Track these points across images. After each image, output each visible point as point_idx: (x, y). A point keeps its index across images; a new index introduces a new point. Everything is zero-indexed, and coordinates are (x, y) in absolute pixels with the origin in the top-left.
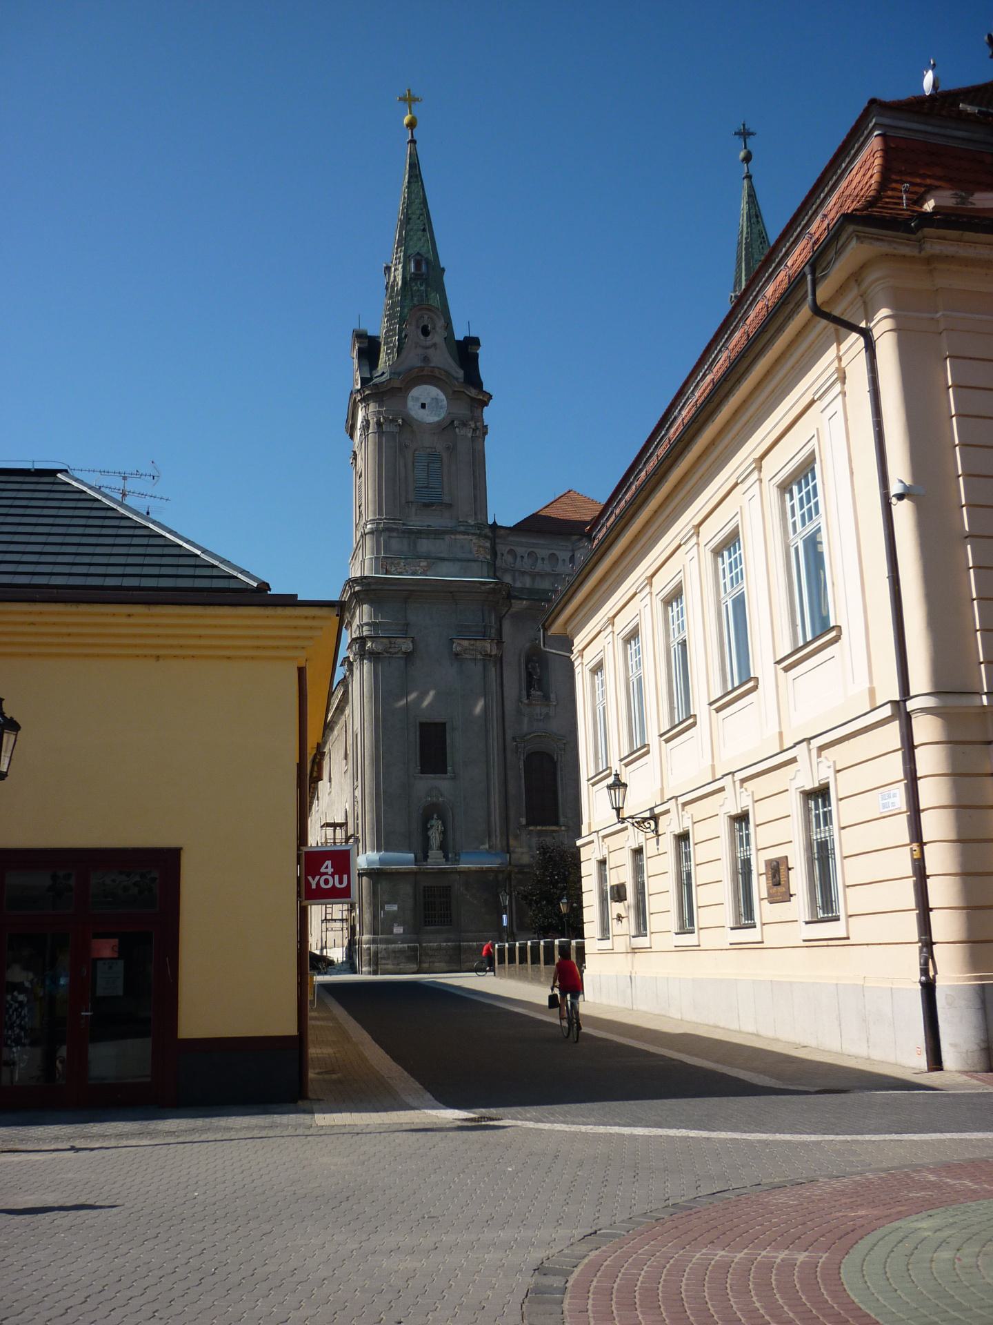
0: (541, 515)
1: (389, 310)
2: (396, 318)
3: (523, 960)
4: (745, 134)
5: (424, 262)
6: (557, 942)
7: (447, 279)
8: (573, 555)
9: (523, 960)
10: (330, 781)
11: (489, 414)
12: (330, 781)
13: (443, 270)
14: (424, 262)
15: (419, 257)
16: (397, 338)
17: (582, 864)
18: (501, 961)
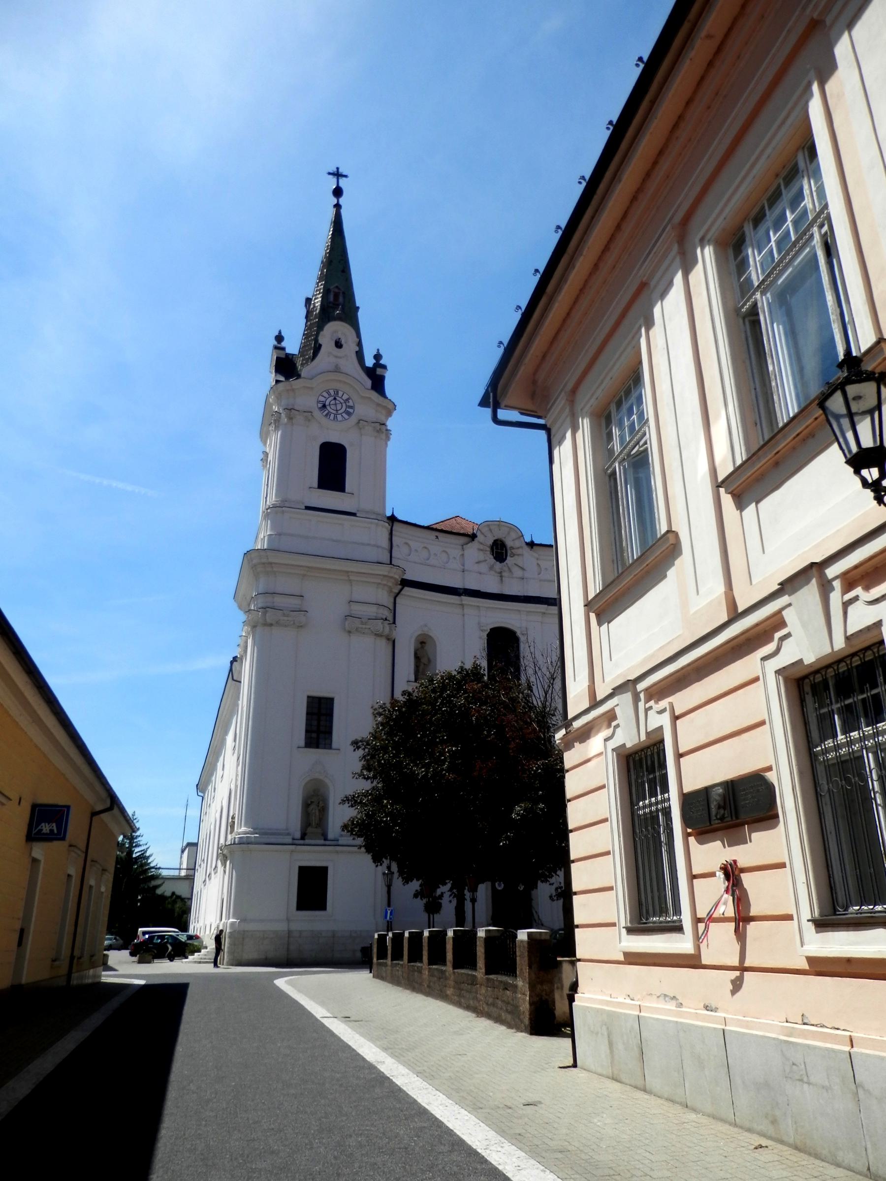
0: (328, 1010)
1: (307, 330)
2: (313, 335)
3: (415, 956)
4: (338, 174)
5: (341, 294)
6: (522, 935)
7: (361, 314)
8: (463, 555)
9: (415, 956)
10: (223, 770)
11: (389, 443)
12: (223, 770)
13: (358, 308)
14: (341, 294)
15: (337, 290)
16: (312, 351)
17: (567, 775)
18: (382, 955)
